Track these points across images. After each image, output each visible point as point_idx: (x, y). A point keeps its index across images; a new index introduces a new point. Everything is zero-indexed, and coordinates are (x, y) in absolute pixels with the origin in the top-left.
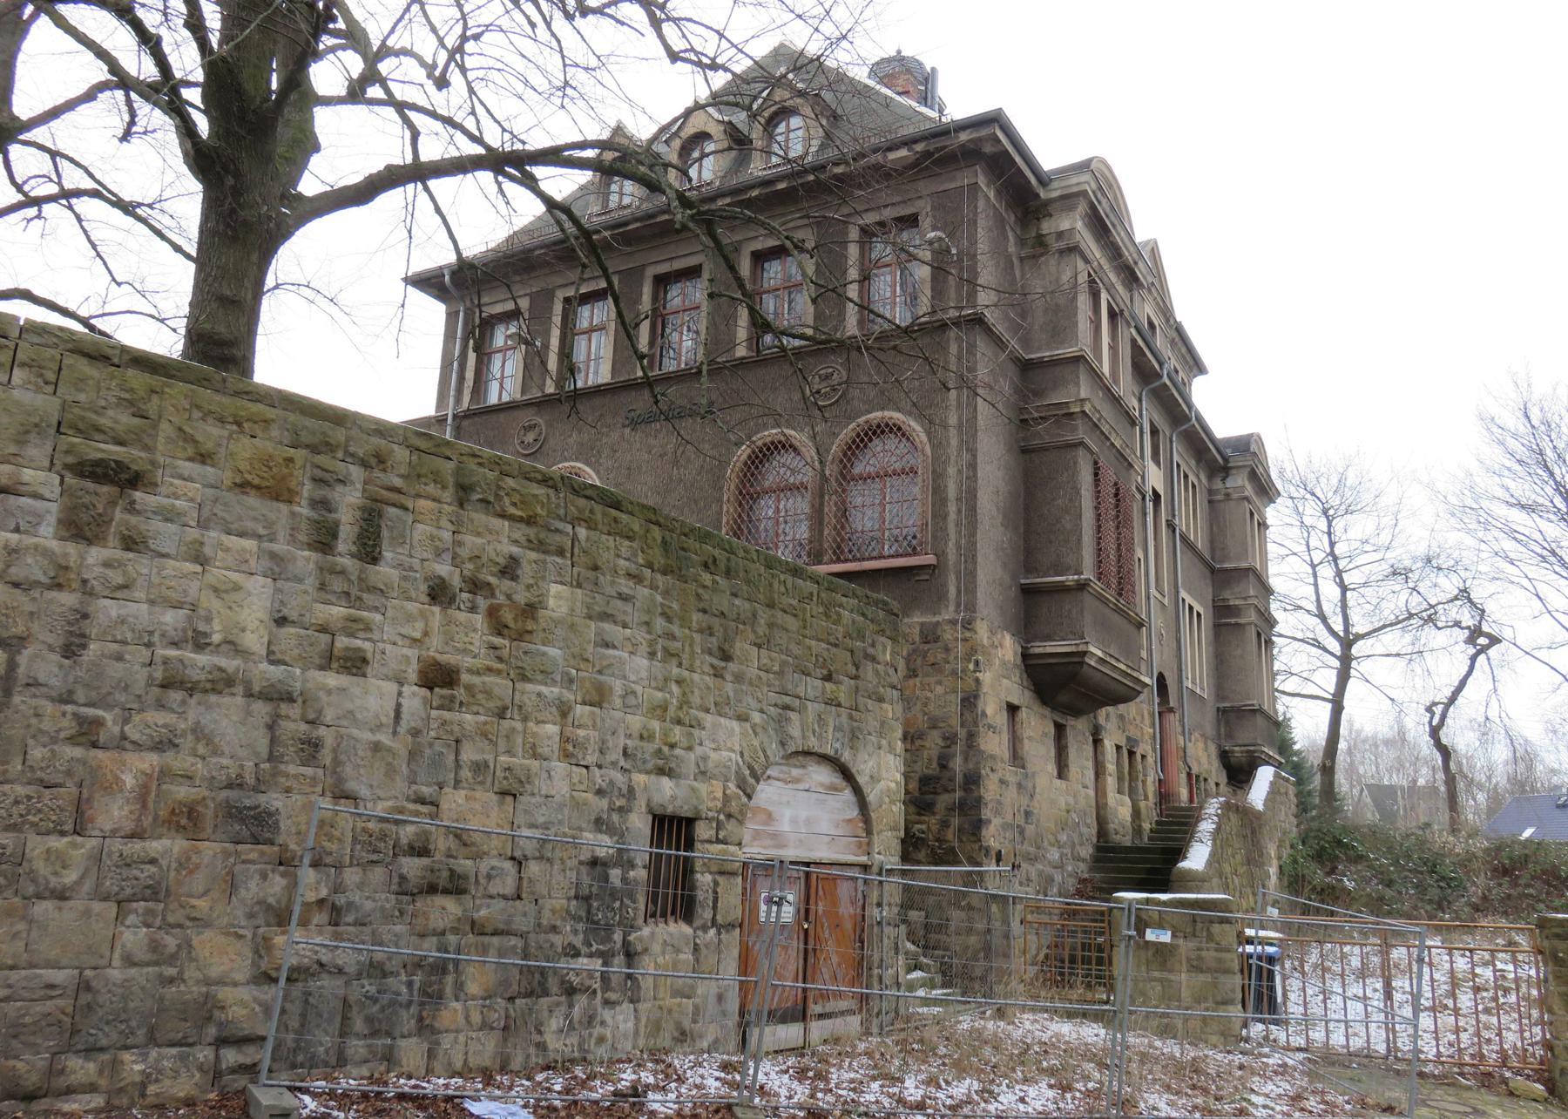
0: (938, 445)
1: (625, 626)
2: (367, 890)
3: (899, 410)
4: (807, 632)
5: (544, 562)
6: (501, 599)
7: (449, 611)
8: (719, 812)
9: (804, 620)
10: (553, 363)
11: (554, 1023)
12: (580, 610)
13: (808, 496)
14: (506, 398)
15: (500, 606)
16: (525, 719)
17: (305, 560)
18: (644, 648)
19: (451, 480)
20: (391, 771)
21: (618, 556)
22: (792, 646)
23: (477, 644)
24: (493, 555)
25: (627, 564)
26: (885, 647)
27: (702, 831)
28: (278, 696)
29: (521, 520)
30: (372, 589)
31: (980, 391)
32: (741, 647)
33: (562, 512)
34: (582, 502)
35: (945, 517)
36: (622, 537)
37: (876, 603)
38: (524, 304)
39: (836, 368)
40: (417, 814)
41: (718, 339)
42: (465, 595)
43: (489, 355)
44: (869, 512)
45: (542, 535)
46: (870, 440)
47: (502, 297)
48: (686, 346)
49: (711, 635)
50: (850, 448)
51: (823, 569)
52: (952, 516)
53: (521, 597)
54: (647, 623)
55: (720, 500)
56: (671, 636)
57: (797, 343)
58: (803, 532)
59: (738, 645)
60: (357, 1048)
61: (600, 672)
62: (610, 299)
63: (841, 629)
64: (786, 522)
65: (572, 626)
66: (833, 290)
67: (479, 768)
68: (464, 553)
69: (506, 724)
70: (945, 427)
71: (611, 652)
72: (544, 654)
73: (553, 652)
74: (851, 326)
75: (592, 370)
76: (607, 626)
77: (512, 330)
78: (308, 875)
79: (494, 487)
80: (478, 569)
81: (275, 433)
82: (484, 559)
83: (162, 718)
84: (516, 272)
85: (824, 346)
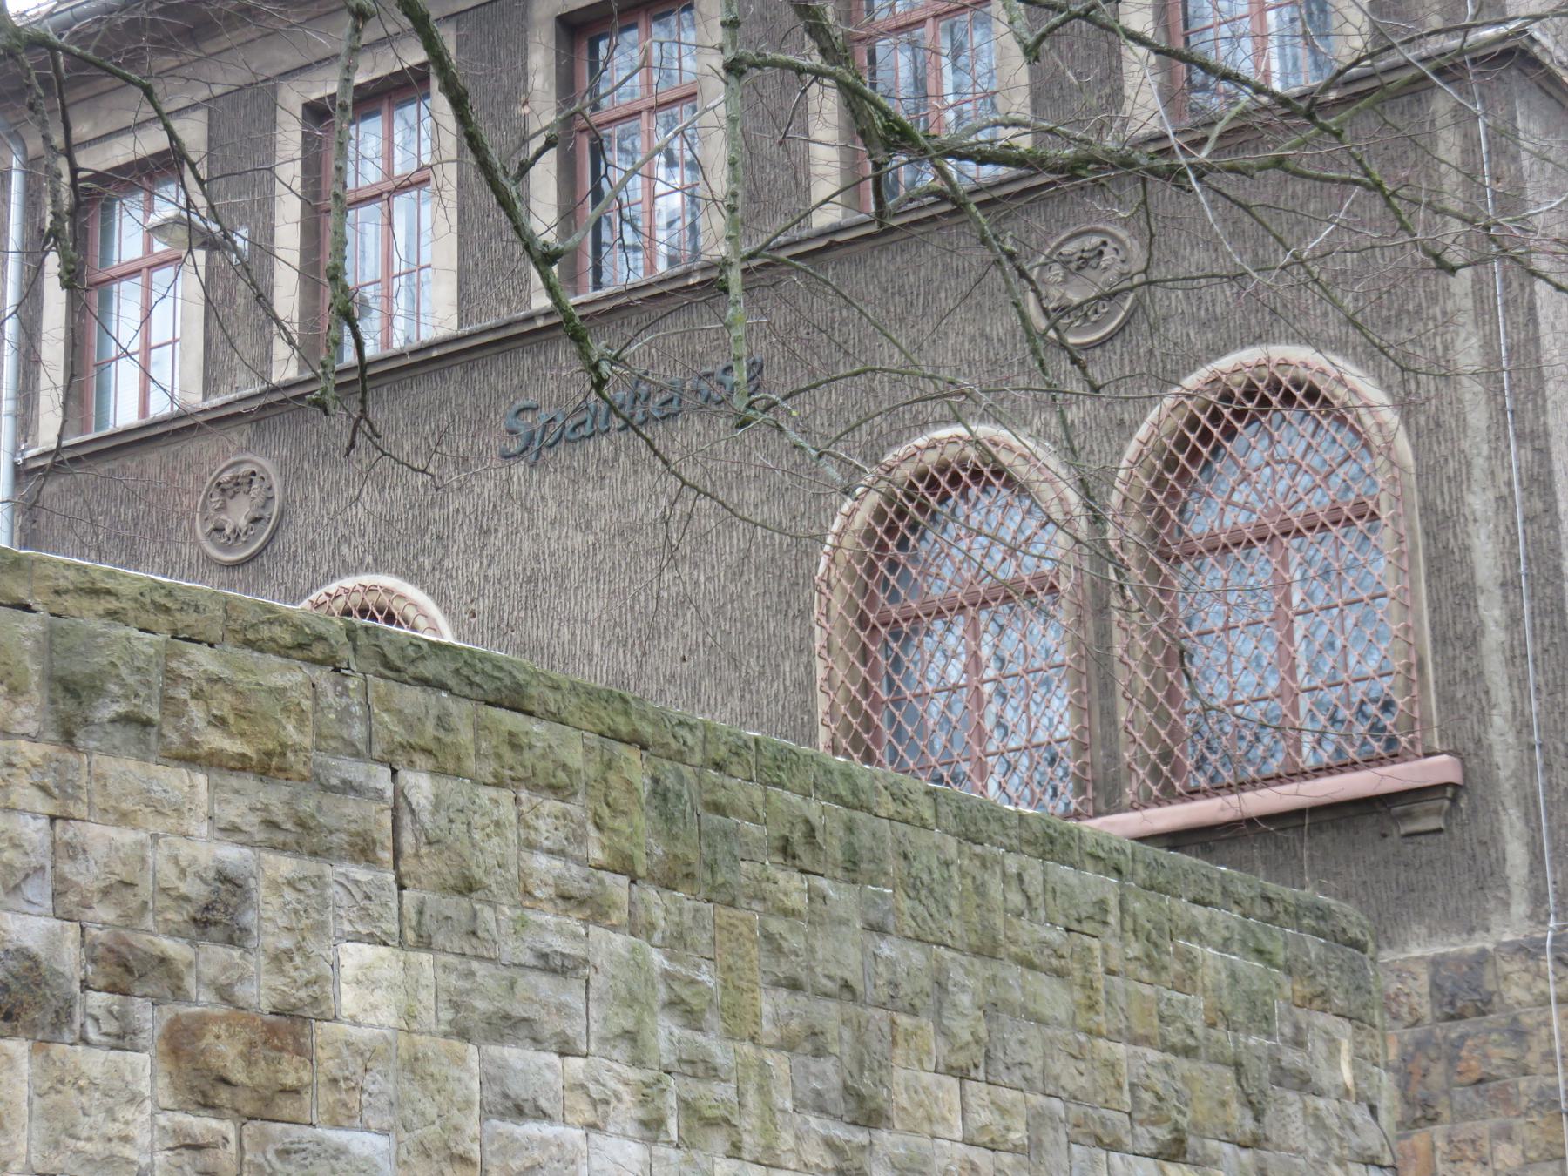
0: (1429, 426)
3: (1307, 339)
4: (1101, 1020)
5: (318, 882)
6: (203, 1001)
7: (57, 1050)
9: (1089, 985)
10: (287, 296)
12: (434, 1014)
13: (1064, 614)
14: (160, 407)
15: (203, 1021)
18: (627, 1111)
19: (33, 670)
21: (530, 846)
22: (1063, 1068)
23: (143, 1139)
24: (169, 875)
25: (557, 864)
26: (1332, 1043)
29: (241, 765)
31: (1542, 264)
32: (912, 1081)
33: (358, 732)
34: (412, 698)
35: (1472, 641)
36: (535, 788)
37: (1296, 914)
38: (193, 132)
39: (1113, 233)
41: (764, 173)
42: (98, 1000)
43: (104, 286)
44: (1245, 645)
45: (307, 806)
46: (1230, 433)
47: (129, 118)
48: (669, 208)
49: (819, 1053)
50: (1171, 464)
51: (1122, 825)
52: (1495, 637)
53: (261, 991)
54: (630, 1036)
55: (803, 648)
56: (706, 1070)
57: (988, 172)
58: (1056, 716)
59: (900, 1075)
62: (440, 102)
63: (1199, 1002)
64: (1005, 698)
65: (413, 1064)
66: (1085, 15)
68: (86, 875)
70: (1449, 376)
71: (532, 1129)
72: (340, 1152)
74: (1144, 103)
75: (401, 304)
76: (515, 1055)
77: (165, 210)
79: (157, 679)
80: (130, 920)
82: (146, 889)
84: (164, 45)
85: (1056, 178)
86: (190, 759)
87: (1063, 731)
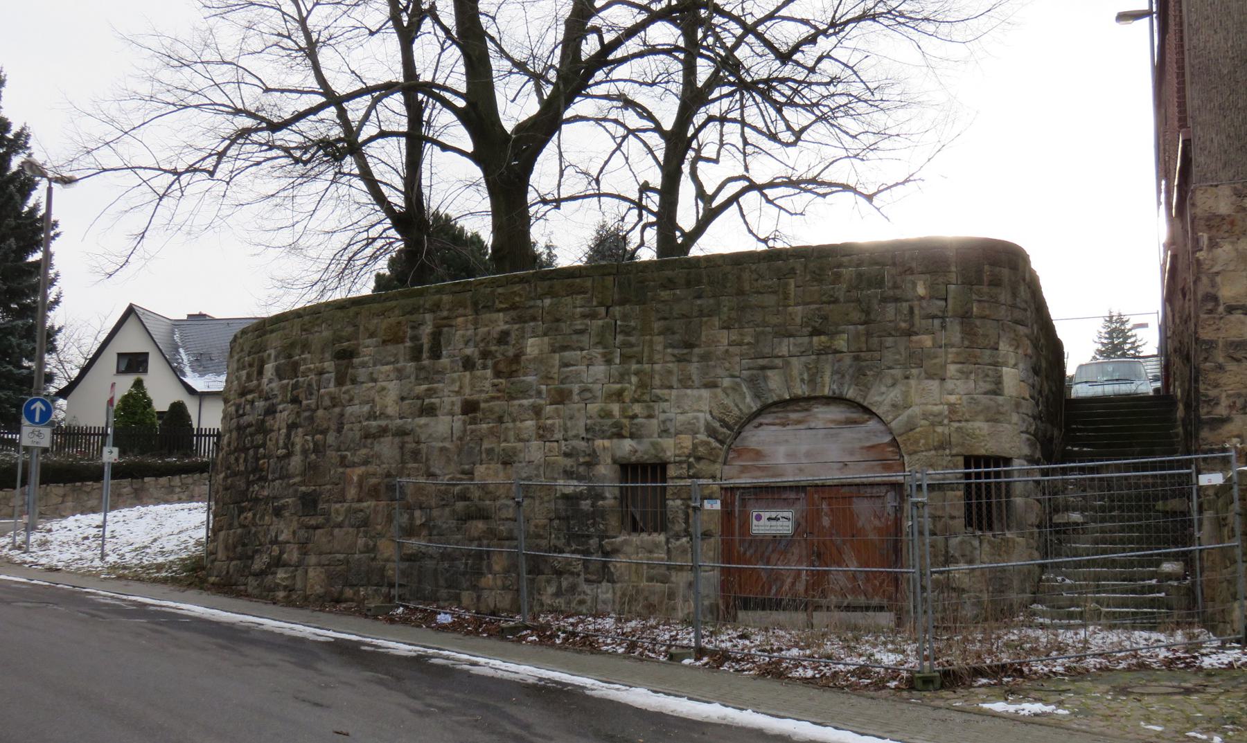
1: (582, 349)
2: (443, 518)
8: (689, 456)
11: (551, 590)
16: (514, 421)
17: (410, 366)
20: (449, 460)
27: (672, 471)
28: (402, 433)
30: (438, 372)
40: (461, 479)
53: (511, 352)
60: (443, 593)
61: (562, 383)
67: (490, 451)
69: (504, 426)
73: (529, 379)
76: (566, 354)
78: (417, 513)
81: (397, 312)
83: (364, 451)
86: (499, 311)
87: (531, 341)
